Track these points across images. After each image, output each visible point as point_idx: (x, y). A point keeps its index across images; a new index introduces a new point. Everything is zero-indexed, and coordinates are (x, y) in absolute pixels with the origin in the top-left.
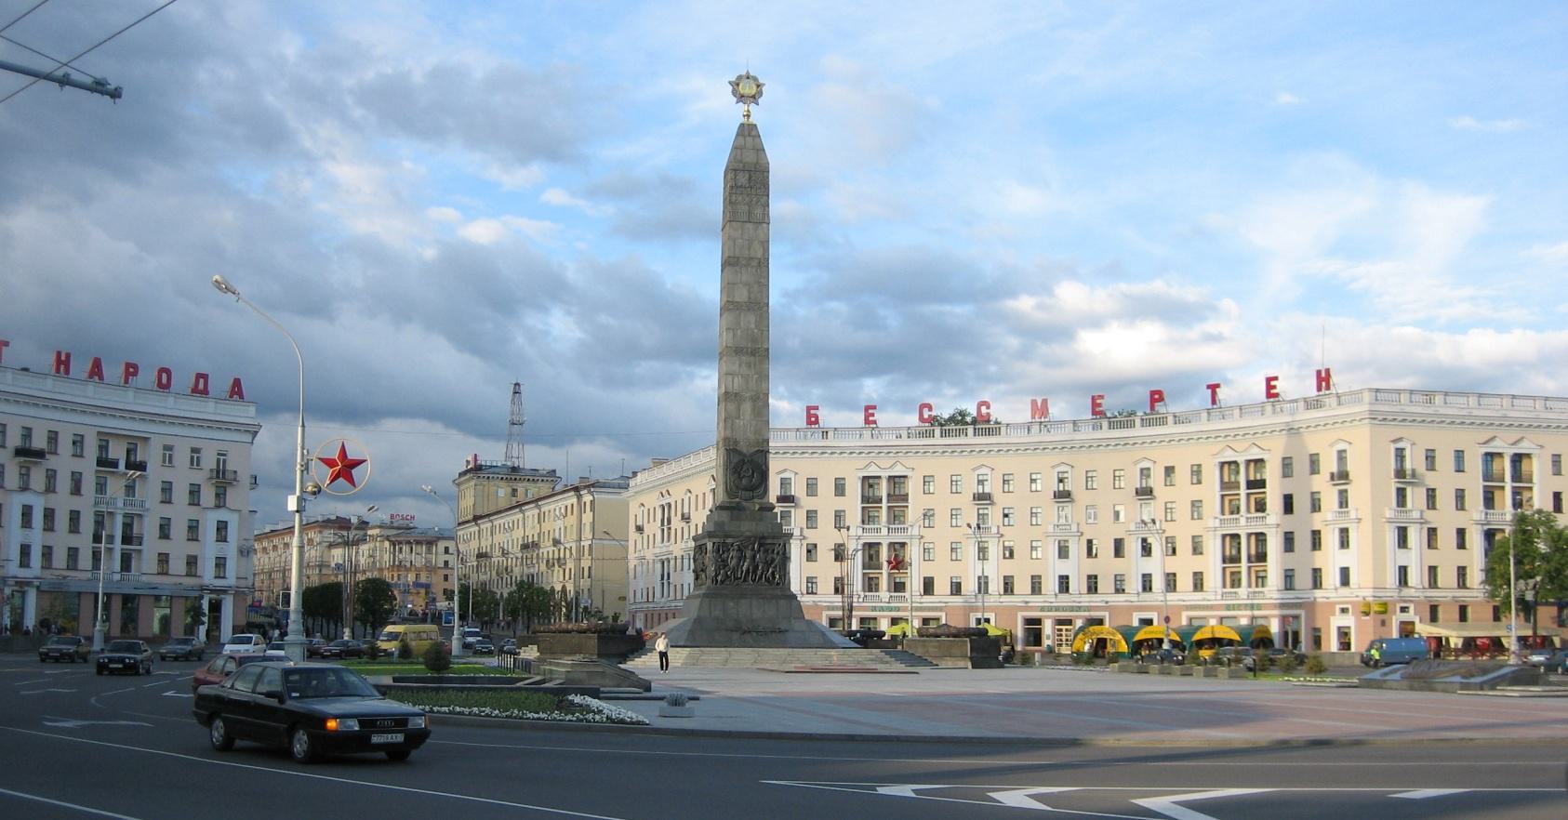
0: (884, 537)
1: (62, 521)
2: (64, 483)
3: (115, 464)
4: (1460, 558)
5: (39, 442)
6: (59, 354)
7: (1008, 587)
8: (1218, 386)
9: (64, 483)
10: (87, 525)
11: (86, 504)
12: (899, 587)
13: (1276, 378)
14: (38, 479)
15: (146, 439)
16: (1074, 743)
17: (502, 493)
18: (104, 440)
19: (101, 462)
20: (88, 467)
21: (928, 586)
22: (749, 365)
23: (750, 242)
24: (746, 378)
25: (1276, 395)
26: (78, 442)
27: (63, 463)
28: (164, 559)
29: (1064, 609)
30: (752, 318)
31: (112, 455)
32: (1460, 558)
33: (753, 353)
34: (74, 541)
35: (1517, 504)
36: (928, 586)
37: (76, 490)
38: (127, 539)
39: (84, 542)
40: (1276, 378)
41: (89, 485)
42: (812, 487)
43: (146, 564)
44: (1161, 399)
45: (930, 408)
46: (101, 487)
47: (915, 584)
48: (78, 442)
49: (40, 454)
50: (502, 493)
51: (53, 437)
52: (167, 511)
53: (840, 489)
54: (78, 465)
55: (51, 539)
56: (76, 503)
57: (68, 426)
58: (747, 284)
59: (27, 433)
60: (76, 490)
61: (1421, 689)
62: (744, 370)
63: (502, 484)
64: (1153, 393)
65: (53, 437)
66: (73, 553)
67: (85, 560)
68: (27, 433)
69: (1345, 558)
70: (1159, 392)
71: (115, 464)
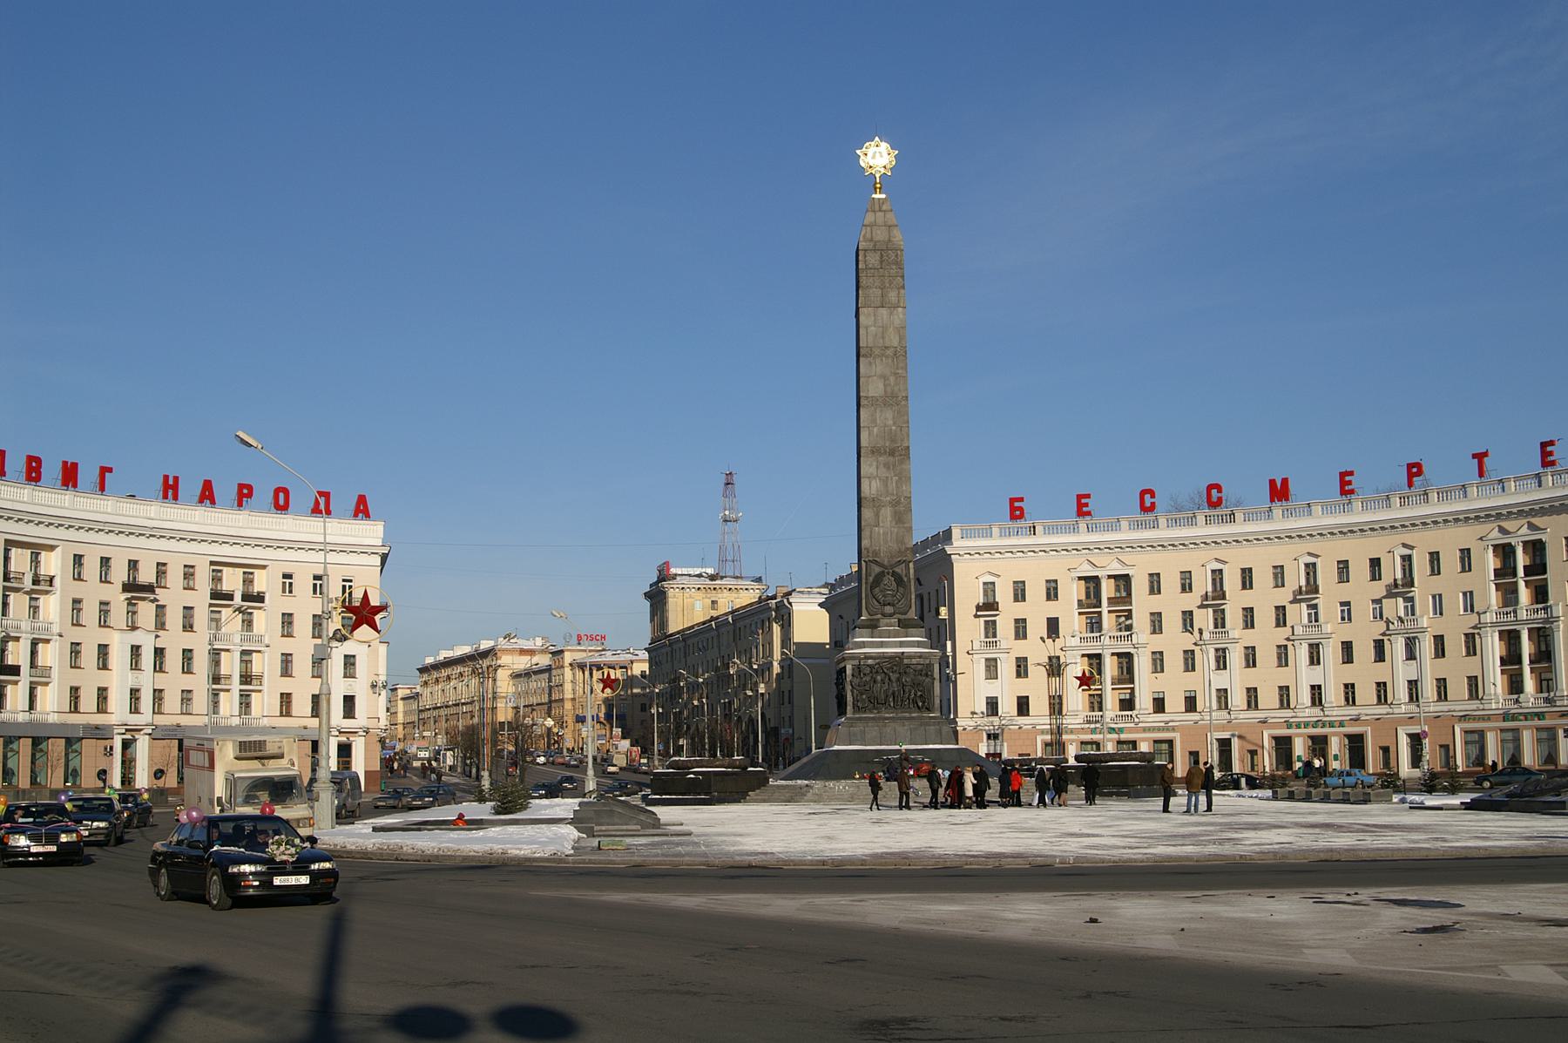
0: (1108, 646)
1: (173, 660)
2: (174, 618)
3: (230, 597)
4: (1471, 666)
5: (146, 575)
6: (166, 478)
7: (1191, 704)
8: (1485, 454)
9: (174, 618)
10: (201, 662)
11: (199, 642)
12: (1128, 704)
13: (1552, 443)
14: (146, 611)
15: (264, 567)
16: (374, 829)
17: (698, 606)
18: (217, 566)
19: (216, 595)
20: (200, 599)
21: (1159, 705)
22: (887, 466)
23: (884, 328)
24: (885, 481)
25: (1553, 463)
26: (189, 573)
27: (173, 596)
28: (286, 698)
29: (1159, 729)
30: (889, 414)
31: (226, 586)
32: (1471, 666)
33: (892, 453)
34: (187, 682)
35: (245, 704)
36: (1159, 705)
37: (188, 627)
38: (246, 678)
39: (199, 682)
40: (1552, 443)
41: (201, 618)
42: (1247, 579)
43: (264, 705)
44: (1419, 473)
45: (1153, 496)
46: (216, 622)
47: (1144, 701)
48: (189, 573)
49: (150, 588)
50: (698, 606)
51: (161, 569)
52: (287, 645)
53: (1052, 592)
54: (189, 598)
55: (161, 681)
56: (188, 641)
57: (177, 555)
58: (884, 377)
59: (133, 565)
60: (188, 627)
61: (1308, 798)
62: (883, 472)
63: (701, 594)
64: (1410, 466)
65: (161, 569)
66: (187, 696)
67: (200, 702)
68: (133, 565)
69: (992, 689)
70: (1418, 465)
71: (230, 597)
